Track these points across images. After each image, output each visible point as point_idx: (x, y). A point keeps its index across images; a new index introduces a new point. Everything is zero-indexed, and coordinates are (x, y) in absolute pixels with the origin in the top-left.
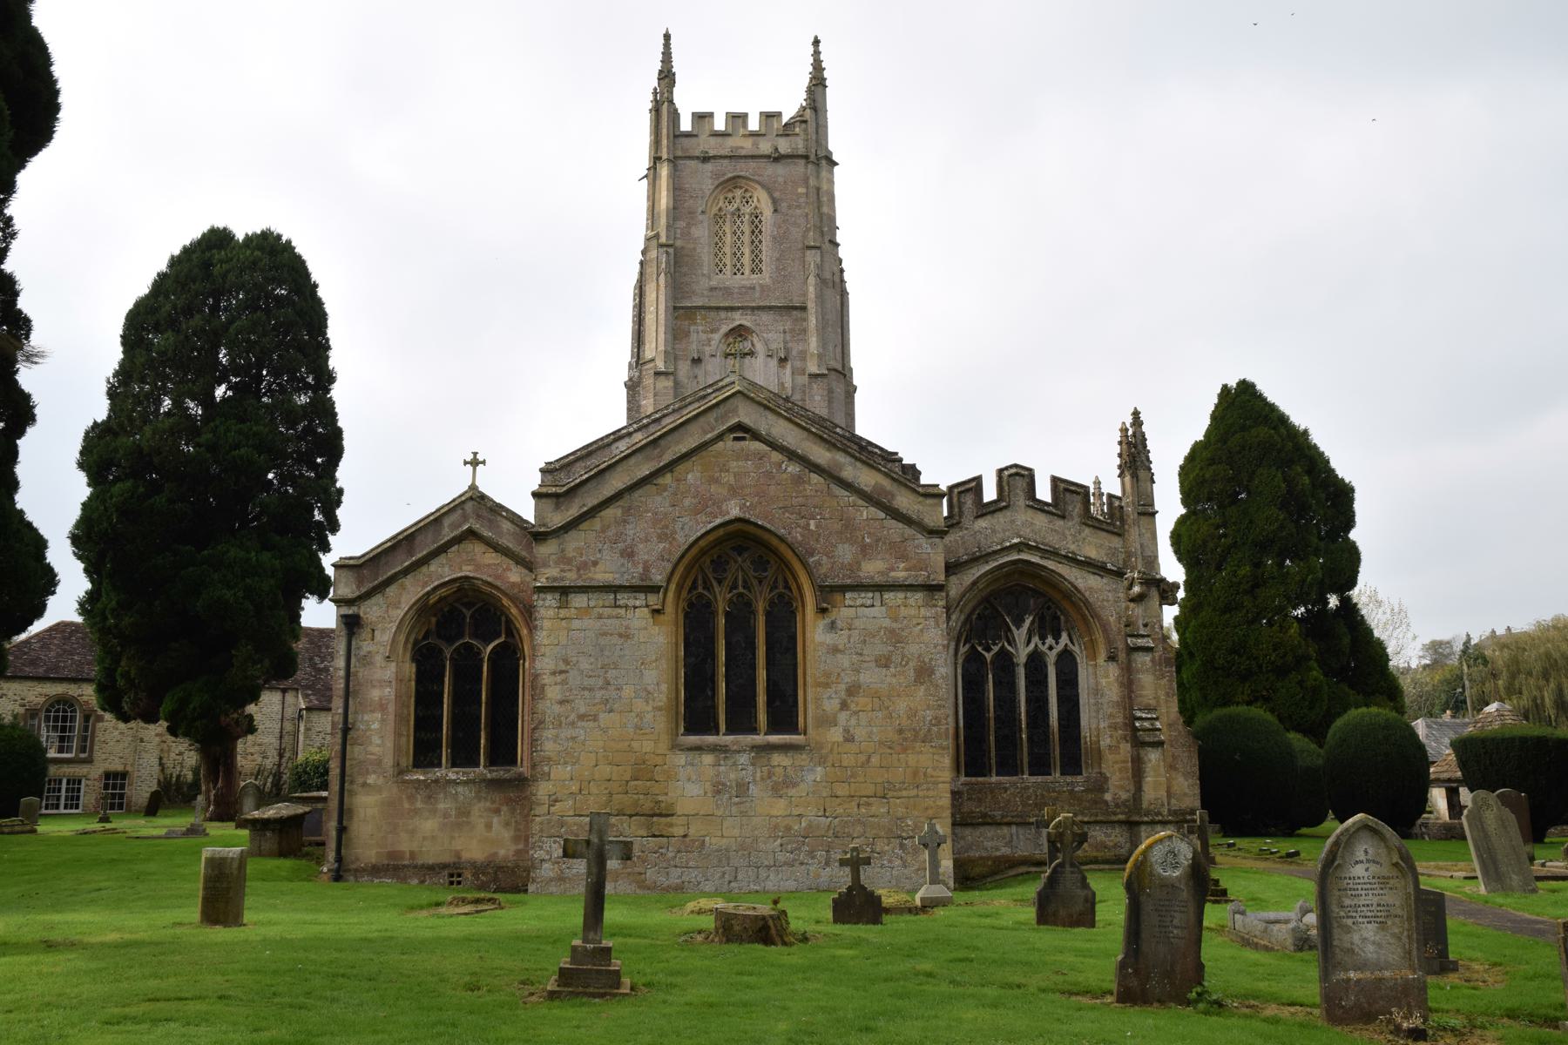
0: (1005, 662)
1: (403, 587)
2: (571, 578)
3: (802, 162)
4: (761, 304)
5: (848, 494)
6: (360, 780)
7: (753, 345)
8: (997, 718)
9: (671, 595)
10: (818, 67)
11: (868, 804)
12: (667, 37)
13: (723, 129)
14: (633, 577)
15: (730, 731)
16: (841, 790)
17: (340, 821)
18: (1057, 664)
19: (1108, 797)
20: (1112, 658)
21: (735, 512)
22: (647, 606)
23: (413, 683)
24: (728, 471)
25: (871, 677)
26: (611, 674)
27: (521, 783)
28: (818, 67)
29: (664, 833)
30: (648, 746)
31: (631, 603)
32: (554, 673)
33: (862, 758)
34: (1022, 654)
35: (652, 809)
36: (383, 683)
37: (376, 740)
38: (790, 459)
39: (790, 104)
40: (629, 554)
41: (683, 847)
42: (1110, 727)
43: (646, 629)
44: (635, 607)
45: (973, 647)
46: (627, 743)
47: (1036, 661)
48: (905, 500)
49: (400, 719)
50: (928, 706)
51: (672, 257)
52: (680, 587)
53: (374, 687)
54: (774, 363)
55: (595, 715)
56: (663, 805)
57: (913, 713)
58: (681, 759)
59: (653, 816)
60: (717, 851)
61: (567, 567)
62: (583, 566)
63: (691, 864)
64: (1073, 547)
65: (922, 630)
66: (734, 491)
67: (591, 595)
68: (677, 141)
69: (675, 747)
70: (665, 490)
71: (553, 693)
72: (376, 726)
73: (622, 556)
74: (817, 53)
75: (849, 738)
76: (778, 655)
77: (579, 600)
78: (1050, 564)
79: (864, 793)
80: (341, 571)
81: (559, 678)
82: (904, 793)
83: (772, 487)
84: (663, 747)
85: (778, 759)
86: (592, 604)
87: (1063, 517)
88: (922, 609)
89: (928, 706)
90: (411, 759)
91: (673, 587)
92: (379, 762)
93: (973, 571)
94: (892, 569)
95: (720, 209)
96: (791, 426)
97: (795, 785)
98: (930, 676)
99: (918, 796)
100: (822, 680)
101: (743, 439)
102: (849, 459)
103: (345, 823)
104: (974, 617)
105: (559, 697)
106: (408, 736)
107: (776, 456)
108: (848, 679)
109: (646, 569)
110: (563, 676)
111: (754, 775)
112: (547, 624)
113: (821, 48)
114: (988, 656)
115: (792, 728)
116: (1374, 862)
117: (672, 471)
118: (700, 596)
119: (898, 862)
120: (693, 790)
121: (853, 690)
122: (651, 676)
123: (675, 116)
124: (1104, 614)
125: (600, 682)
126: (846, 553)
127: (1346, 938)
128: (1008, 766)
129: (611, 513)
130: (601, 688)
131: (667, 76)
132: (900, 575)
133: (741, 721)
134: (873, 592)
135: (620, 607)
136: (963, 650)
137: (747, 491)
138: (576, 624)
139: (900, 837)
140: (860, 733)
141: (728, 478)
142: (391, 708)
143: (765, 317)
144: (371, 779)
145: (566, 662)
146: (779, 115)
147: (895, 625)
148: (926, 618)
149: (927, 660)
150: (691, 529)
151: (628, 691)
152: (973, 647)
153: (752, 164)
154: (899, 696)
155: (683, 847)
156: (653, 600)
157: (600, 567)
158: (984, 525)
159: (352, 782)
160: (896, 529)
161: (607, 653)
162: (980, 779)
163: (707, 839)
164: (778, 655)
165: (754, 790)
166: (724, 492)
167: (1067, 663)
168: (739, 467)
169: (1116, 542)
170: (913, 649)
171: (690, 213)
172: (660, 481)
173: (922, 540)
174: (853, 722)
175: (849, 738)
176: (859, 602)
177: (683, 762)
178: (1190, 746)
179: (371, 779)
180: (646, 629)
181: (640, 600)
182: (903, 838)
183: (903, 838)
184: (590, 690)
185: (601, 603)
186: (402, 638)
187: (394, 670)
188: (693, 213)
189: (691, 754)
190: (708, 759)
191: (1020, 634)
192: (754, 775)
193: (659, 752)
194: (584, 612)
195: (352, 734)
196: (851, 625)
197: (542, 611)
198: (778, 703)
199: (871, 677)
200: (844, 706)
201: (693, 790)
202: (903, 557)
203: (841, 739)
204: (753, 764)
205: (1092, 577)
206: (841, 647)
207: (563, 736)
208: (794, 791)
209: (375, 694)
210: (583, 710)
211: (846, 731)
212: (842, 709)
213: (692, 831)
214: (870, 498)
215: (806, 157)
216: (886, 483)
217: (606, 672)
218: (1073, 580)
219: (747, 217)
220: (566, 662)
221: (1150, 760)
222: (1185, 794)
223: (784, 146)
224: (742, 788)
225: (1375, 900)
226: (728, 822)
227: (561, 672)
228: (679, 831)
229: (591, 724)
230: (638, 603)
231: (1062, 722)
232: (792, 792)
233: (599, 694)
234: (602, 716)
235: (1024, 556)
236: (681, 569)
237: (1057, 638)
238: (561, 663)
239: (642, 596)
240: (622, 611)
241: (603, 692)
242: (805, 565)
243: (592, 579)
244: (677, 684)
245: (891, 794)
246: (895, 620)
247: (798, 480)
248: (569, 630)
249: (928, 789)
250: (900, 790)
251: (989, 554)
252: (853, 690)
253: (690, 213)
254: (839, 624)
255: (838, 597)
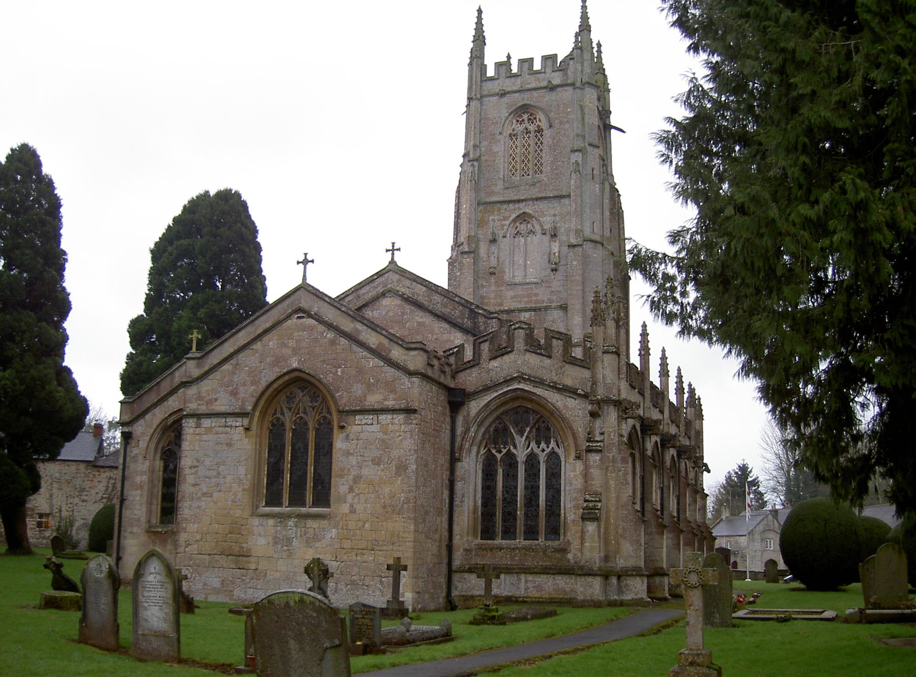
0: (511, 462)
1: (154, 415)
2: (203, 409)
3: (570, 89)
4: (540, 196)
5: (361, 350)
6: (129, 530)
7: (533, 226)
8: (504, 500)
9: (256, 419)
10: (585, 17)
11: (363, 554)
12: (480, 11)
13: (540, 68)
14: (236, 408)
15: (290, 505)
16: (347, 544)
17: (118, 553)
18: (547, 462)
19: (570, 556)
20: (578, 457)
21: (295, 365)
22: (242, 426)
23: (161, 473)
24: (293, 339)
25: (369, 471)
26: (222, 468)
27: (174, 533)
28: (585, 17)
29: (245, 567)
30: (238, 513)
31: (234, 424)
32: (191, 468)
33: (361, 524)
34: (521, 455)
35: (239, 552)
36: (143, 473)
37: (138, 507)
38: (329, 329)
39: (563, 48)
40: (234, 393)
41: (254, 576)
42: (574, 507)
43: (241, 440)
44: (236, 427)
45: (489, 449)
46: (227, 511)
47: (532, 460)
48: (396, 353)
49: (151, 495)
50: (403, 490)
51: (476, 168)
52: (263, 414)
53: (137, 475)
54: (546, 238)
55: (211, 494)
56: (245, 549)
57: (392, 496)
58: (256, 521)
59: (239, 556)
60: (274, 579)
61: (201, 403)
62: (210, 402)
63: (258, 587)
64: (555, 379)
65: (401, 440)
66: (295, 351)
67: (213, 419)
68: (484, 84)
69: (254, 514)
70: (257, 352)
71: (190, 479)
72: (138, 498)
73: (231, 395)
74: (479, 18)
75: (353, 511)
76: (322, 457)
77: (206, 423)
78: (539, 391)
79: (361, 547)
80: (124, 405)
81: (193, 470)
82: (384, 548)
83: (318, 348)
84: (246, 514)
85: (310, 523)
86: (213, 425)
87: (550, 357)
88: (403, 426)
89: (403, 490)
90: (159, 518)
91: (257, 414)
92: (139, 520)
93: (486, 397)
94: (386, 400)
95: (513, 130)
96: (332, 307)
97: (319, 540)
98: (405, 471)
99: (393, 550)
100: (339, 473)
101: (303, 317)
102: (365, 327)
103: (120, 555)
104: (492, 429)
105: (193, 482)
106: (157, 504)
107: (321, 328)
108: (354, 473)
109: (243, 403)
110: (196, 469)
111: (296, 533)
112: (189, 437)
113: (602, 49)
114: (499, 456)
115: (327, 505)
116: (159, 574)
117: (261, 340)
118: (301, 418)
119: (378, 593)
120: (262, 541)
121: (357, 479)
122: (242, 470)
123: (483, 68)
124: (574, 426)
125: (215, 473)
126: (358, 389)
127: (145, 613)
128: (509, 533)
129: (227, 367)
130: (216, 477)
131: (479, 39)
132: (390, 403)
133: (297, 499)
134: (373, 414)
135: (228, 427)
136: (482, 451)
137: (302, 351)
138: (205, 437)
139: (380, 576)
140: (359, 507)
141: (292, 343)
142: (146, 487)
143: (542, 205)
144: (135, 530)
145: (198, 461)
146: (555, 56)
147: (386, 437)
148: (405, 432)
149: (404, 460)
150: (268, 376)
151: (229, 479)
152: (489, 449)
153: (535, 94)
154: (385, 483)
155: (254, 576)
156: (246, 421)
157: (218, 403)
158: (496, 365)
159: (125, 531)
160: (390, 372)
161: (219, 455)
162: (489, 542)
163: (268, 572)
164: (322, 457)
165: (295, 542)
166: (289, 352)
167: (554, 461)
168: (299, 336)
169: (586, 374)
170: (395, 453)
171: (491, 135)
172: (254, 347)
173: (405, 379)
174: (356, 500)
175: (353, 511)
176: (364, 421)
177: (257, 524)
178: (636, 522)
179: (135, 530)
180: (241, 440)
181: (239, 422)
182: (382, 577)
183: (382, 577)
184: (210, 478)
185: (218, 424)
186: (153, 446)
187: (148, 464)
188: (494, 134)
189: (261, 519)
190: (271, 522)
191: (520, 441)
192: (296, 533)
193: (244, 517)
194: (209, 430)
195: (126, 502)
196: (358, 436)
197: (187, 429)
198: (320, 488)
199: (369, 471)
200: (351, 489)
201: (262, 541)
202: (393, 391)
203: (348, 512)
204: (296, 526)
205: (568, 399)
206: (351, 451)
207: (193, 505)
208: (319, 544)
209: (138, 479)
210: (205, 490)
211: (352, 506)
212: (349, 492)
213: (260, 567)
214: (374, 352)
215: (573, 85)
216: (386, 342)
217: (218, 467)
218: (554, 401)
219: (532, 133)
220: (198, 461)
221: (588, 531)
222: (630, 556)
223: (557, 79)
224: (289, 541)
225: (159, 594)
226: (280, 562)
227: (195, 467)
228: (253, 566)
229: (209, 499)
230: (238, 424)
231: (548, 503)
232: (318, 545)
233: (214, 480)
234: (215, 494)
235: (521, 386)
236: (262, 402)
237: (548, 443)
238: (195, 461)
239: (240, 419)
240: (228, 429)
241: (216, 479)
242: (332, 396)
243: (213, 409)
244: (259, 475)
245: (376, 548)
246: (385, 433)
247: (333, 342)
248: (201, 441)
249: (399, 546)
250: (382, 546)
251: (496, 385)
252: (357, 479)
253: (491, 135)
254: (352, 436)
255: (351, 418)
